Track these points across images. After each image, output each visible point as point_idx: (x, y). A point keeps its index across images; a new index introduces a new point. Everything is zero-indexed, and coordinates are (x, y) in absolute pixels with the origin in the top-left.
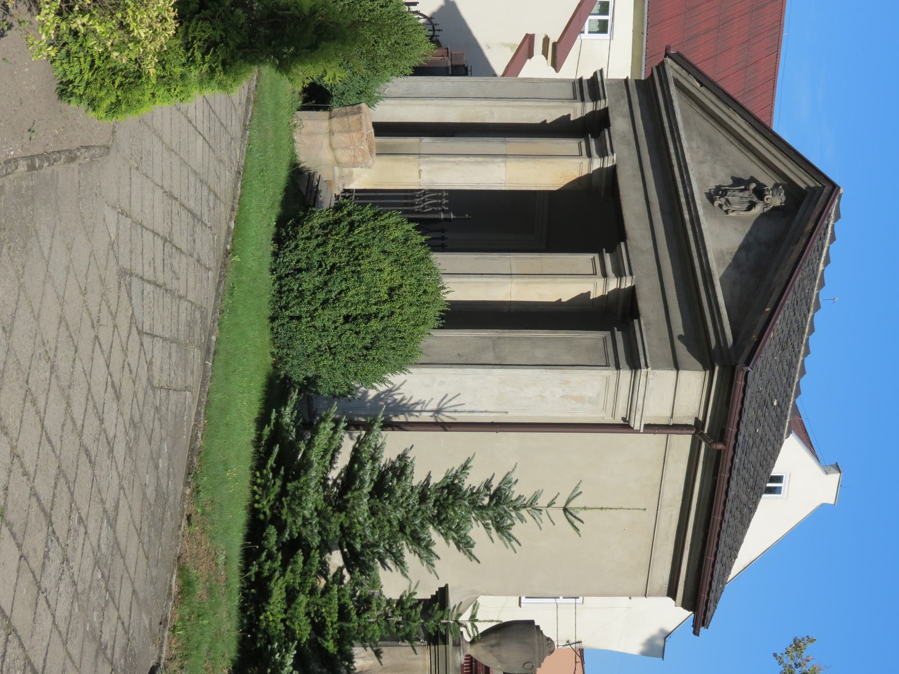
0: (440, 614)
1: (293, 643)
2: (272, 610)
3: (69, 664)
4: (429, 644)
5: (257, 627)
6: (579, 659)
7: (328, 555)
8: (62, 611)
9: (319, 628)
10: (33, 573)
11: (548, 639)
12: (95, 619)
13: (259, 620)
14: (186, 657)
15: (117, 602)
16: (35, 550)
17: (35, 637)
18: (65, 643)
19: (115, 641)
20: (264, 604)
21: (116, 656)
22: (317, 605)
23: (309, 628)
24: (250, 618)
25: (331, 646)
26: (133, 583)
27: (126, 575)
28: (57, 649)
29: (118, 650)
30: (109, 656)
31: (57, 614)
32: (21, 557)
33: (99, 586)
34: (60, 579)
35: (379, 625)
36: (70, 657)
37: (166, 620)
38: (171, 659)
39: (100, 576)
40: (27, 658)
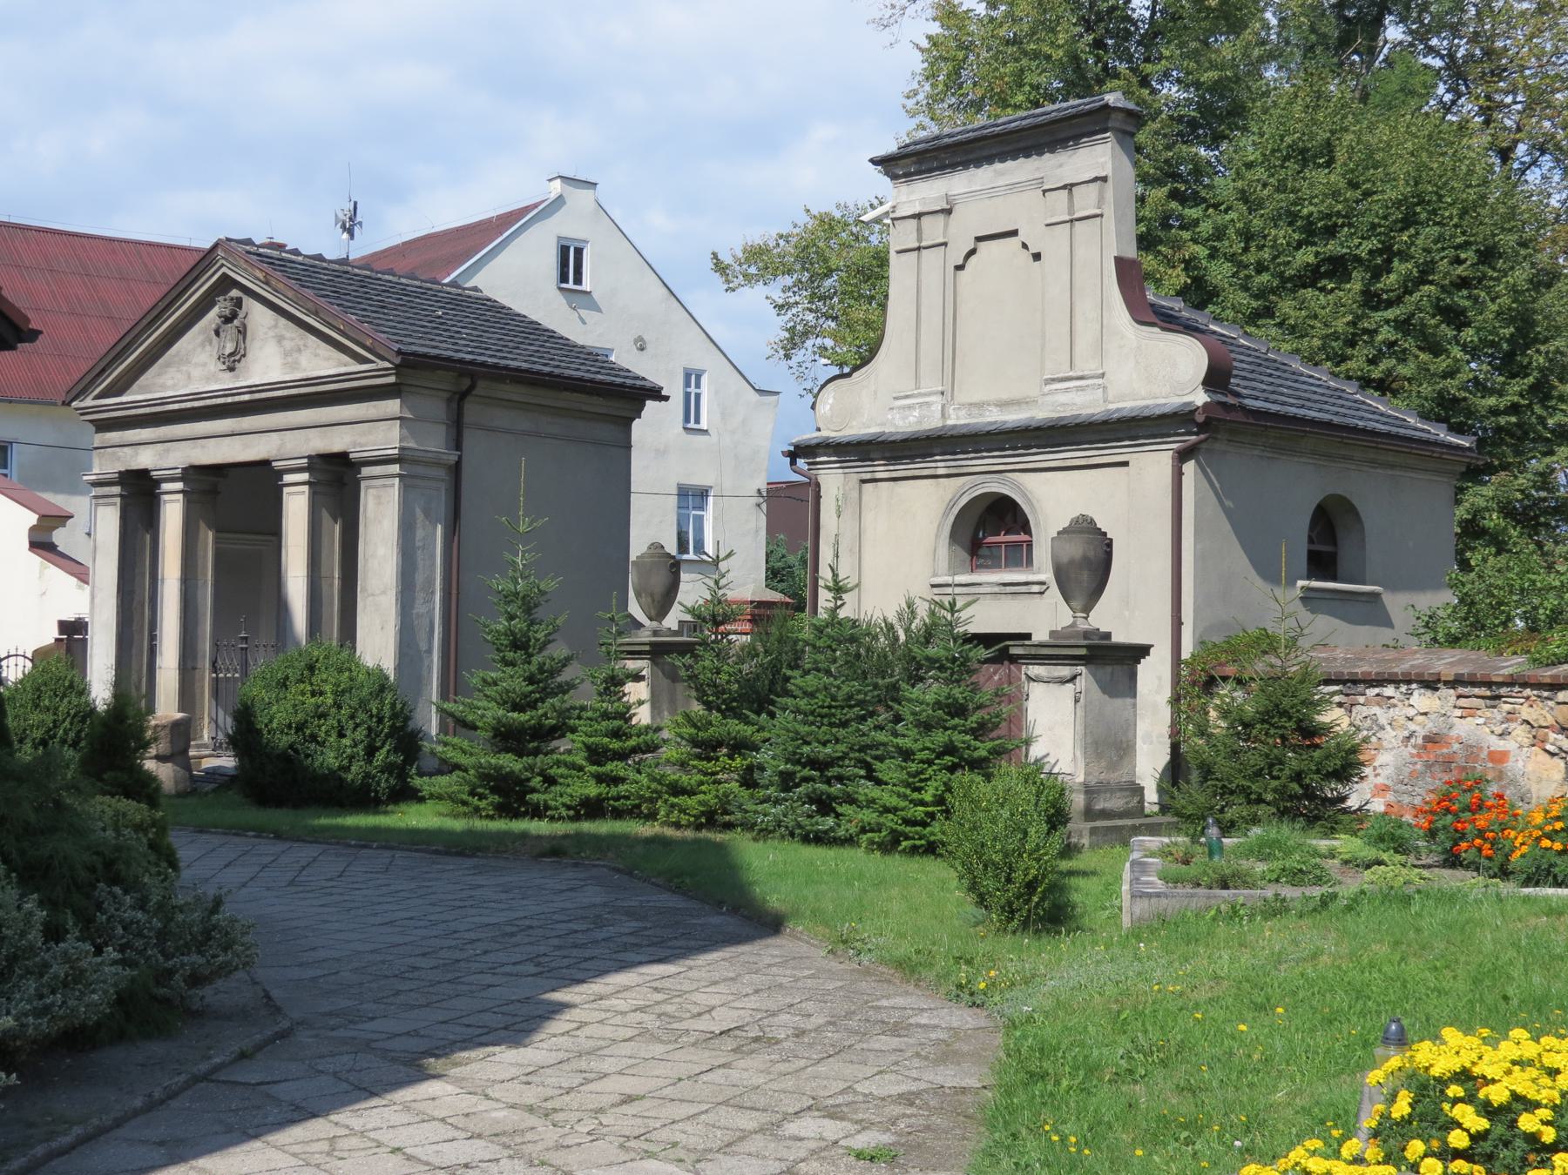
7: (1091, 554)
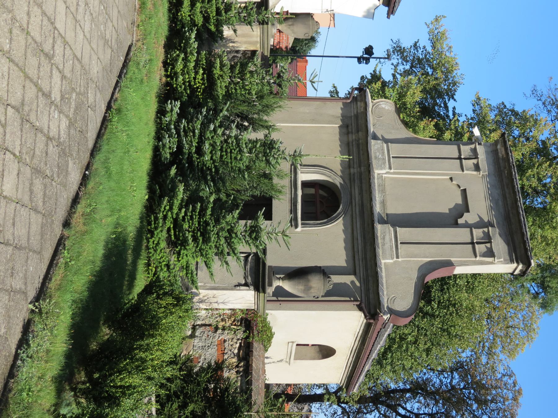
0: (265, 12)
1: (195, 28)
2: (184, 11)
3: (92, 52)
4: (259, 24)
5: (177, 19)
6: (332, 19)
8: (87, 29)
9: (206, 19)
10: (73, 14)
11: (317, 22)
12: (102, 29)
13: (178, 15)
14: (145, 39)
15: (111, 18)
16: (72, 3)
17: (76, 44)
18: (90, 43)
19: (112, 37)
20: (180, 8)
21: (113, 44)
22: (206, 8)
23: (202, 19)
24: (173, 14)
25: (213, 28)
26: (118, 8)
27: (114, 4)
28: (87, 47)
29: (113, 41)
30: (110, 45)
31: (85, 31)
32: (67, 7)
33: (103, 13)
34: (85, 14)
35: (235, 17)
36: (93, 49)
37: (134, 22)
38: (137, 41)
39: (102, 8)
40: (74, 54)
